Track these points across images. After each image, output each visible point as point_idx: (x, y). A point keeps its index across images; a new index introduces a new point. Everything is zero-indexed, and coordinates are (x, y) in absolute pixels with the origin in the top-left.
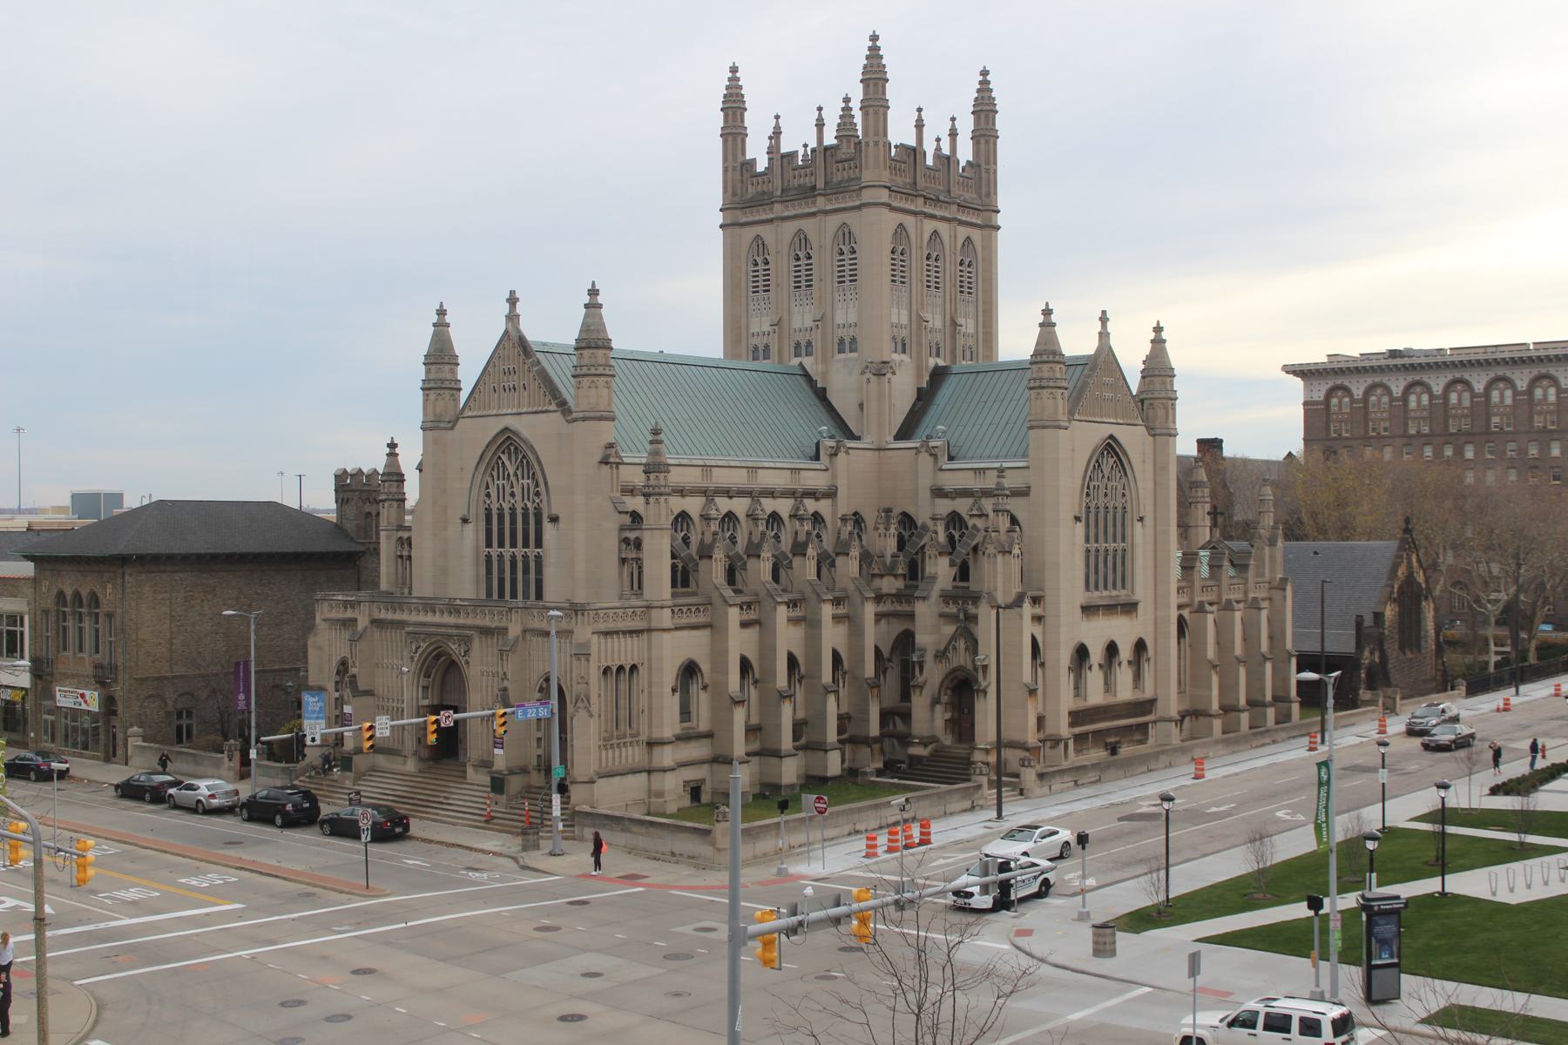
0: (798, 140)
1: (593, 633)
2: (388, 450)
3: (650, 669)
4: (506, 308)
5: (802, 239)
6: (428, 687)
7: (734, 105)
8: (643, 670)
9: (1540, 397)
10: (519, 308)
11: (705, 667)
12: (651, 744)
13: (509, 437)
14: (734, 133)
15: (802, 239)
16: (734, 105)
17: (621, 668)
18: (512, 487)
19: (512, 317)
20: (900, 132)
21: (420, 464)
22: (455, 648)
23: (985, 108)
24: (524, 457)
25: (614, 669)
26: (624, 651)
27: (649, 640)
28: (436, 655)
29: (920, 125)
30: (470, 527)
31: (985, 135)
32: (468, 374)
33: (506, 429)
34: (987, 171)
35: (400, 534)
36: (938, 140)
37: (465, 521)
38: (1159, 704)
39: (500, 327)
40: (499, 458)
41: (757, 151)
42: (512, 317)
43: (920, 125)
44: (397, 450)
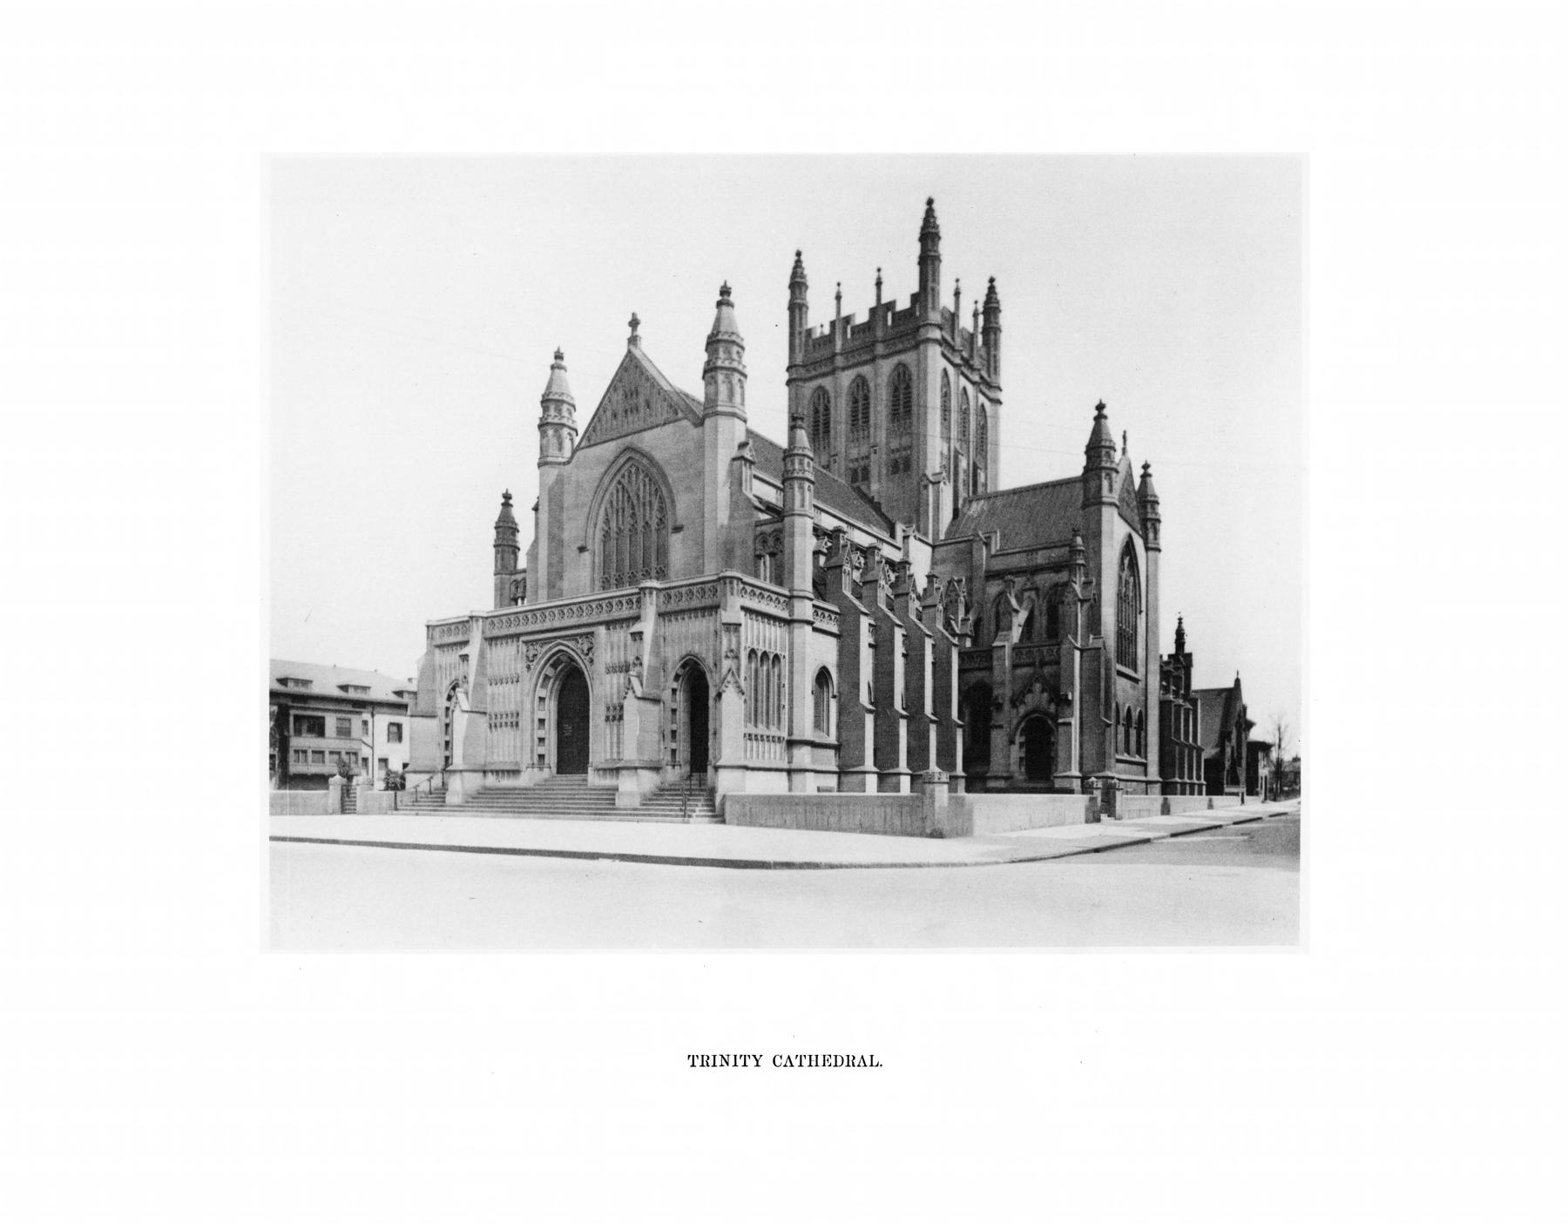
3: (791, 662)
4: (628, 332)
5: (861, 383)
6: (550, 678)
7: (797, 284)
8: (785, 664)
9: (1056, 786)
10: (640, 331)
12: (791, 744)
13: (630, 459)
14: (796, 308)
15: (861, 383)
16: (797, 284)
17: (765, 654)
18: (633, 508)
19: (633, 340)
20: (946, 300)
21: (537, 505)
22: (575, 649)
23: (991, 308)
24: (647, 475)
25: (759, 654)
26: (769, 637)
27: (791, 633)
28: (555, 662)
29: (957, 294)
30: (586, 556)
31: (991, 330)
32: (582, 418)
33: (628, 449)
35: (513, 577)
36: (976, 302)
37: (582, 549)
38: (1111, 820)
40: (619, 483)
42: (633, 340)
43: (957, 294)
44: (511, 502)
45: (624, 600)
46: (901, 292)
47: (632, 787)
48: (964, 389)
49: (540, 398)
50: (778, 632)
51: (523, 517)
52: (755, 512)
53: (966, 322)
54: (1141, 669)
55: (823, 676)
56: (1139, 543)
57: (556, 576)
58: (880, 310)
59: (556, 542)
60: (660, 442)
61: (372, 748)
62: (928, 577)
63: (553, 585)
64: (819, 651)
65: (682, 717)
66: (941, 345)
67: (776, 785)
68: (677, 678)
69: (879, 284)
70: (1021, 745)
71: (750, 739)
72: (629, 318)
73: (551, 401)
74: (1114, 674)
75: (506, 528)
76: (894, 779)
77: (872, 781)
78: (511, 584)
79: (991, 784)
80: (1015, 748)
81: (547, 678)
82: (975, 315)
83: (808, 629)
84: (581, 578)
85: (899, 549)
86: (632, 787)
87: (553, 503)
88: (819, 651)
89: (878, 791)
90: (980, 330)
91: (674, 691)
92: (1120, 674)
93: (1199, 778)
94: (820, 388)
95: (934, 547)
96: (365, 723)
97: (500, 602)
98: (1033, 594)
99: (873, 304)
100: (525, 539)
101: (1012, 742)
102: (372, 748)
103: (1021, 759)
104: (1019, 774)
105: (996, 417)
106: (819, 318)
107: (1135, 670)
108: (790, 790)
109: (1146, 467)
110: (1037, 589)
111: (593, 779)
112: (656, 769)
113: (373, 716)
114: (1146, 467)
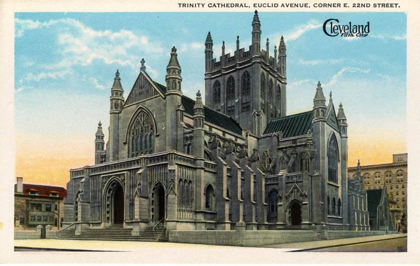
0: (231, 51)
1: (176, 164)
2: (98, 126)
5: (231, 79)
7: (209, 43)
11: (214, 187)
14: (209, 53)
15: (231, 79)
16: (209, 43)
19: (143, 68)
20: (263, 47)
29: (268, 44)
31: (283, 57)
32: (125, 96)
34: (283, 67)
36: (275, 47)
37: (125, 143)
39: (138, 72)
41: (217, 55)
42: (143, 68)
43: (268, 44)
45: (113, 166)
46: (246, 45)
47: (136, 230)
48: (271, 79)
49: (164, 78)
50: (191, 172)
51: (106, 131)
52: (185, 129)
53: (271, 54)
54: (339, 181)
55: (209, 188)
56: (337, 135)
57: (116, 152)
58: (239, 51)
59: (116, 141)
60: (150, 104)
61: (58, 215)
62: (254, 150)
63: (116, 157)
64: (206, 177)
65: (156, 203)
66: (260, 64)
67: (190, 228)
68: (154, 189)
69: (238, 42)
70: (290, 212)
71: (180, 211)
72: (141, 60)
73: (117, 90)
74: (327, 186)
75: (100, 136)
76: (223, 225)
77: (228, 226)
78: (101, 158)
79: (278, 227)
80: (287, 213)
81: (110, 190)
82: (275, 51)
83: (203, 171)
84: (124, 156)
85: (244, 140)
86: (136, 230)
87: (115, 129)
88: (206, 177)
89: (231, 229)
90: (277, 57)
91: (153, 194)
92: (328, 184)
93: (366, 223)
94: (231, 76)
95: (258, 139)
96: (56, 206)
97: (96, 163)
98: (295, 155)
99: (221, 55)
100: (106, 140)
101: (286, 211)
102: (58, 215)
103: (290, 217)
104: (289, 224)
105: (285, 88)
106: (217, 55)
107: (337, 184)
108: (196, 229)
109: (341, 106)
110: (297, 154)
111: (125, 226)
112: (147, 222)
113: (59, 203)
114: (341, 106)
